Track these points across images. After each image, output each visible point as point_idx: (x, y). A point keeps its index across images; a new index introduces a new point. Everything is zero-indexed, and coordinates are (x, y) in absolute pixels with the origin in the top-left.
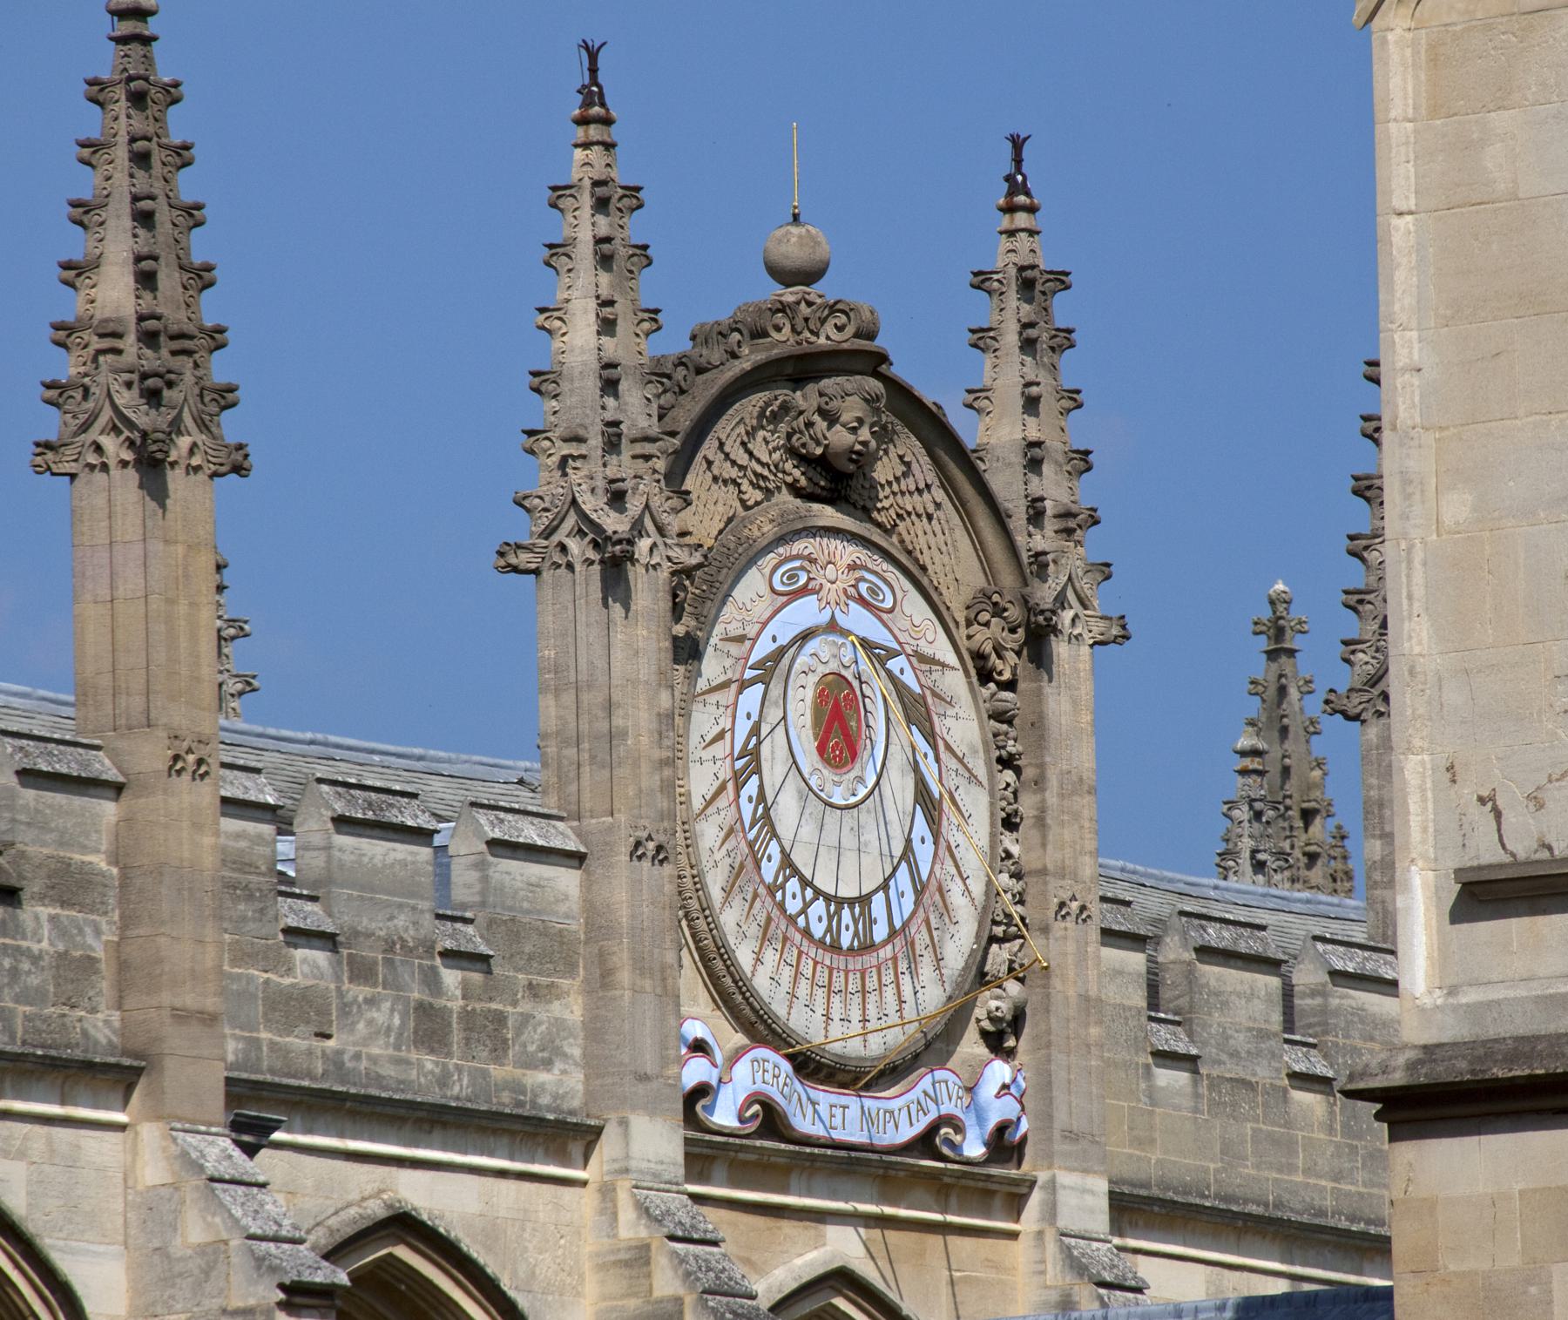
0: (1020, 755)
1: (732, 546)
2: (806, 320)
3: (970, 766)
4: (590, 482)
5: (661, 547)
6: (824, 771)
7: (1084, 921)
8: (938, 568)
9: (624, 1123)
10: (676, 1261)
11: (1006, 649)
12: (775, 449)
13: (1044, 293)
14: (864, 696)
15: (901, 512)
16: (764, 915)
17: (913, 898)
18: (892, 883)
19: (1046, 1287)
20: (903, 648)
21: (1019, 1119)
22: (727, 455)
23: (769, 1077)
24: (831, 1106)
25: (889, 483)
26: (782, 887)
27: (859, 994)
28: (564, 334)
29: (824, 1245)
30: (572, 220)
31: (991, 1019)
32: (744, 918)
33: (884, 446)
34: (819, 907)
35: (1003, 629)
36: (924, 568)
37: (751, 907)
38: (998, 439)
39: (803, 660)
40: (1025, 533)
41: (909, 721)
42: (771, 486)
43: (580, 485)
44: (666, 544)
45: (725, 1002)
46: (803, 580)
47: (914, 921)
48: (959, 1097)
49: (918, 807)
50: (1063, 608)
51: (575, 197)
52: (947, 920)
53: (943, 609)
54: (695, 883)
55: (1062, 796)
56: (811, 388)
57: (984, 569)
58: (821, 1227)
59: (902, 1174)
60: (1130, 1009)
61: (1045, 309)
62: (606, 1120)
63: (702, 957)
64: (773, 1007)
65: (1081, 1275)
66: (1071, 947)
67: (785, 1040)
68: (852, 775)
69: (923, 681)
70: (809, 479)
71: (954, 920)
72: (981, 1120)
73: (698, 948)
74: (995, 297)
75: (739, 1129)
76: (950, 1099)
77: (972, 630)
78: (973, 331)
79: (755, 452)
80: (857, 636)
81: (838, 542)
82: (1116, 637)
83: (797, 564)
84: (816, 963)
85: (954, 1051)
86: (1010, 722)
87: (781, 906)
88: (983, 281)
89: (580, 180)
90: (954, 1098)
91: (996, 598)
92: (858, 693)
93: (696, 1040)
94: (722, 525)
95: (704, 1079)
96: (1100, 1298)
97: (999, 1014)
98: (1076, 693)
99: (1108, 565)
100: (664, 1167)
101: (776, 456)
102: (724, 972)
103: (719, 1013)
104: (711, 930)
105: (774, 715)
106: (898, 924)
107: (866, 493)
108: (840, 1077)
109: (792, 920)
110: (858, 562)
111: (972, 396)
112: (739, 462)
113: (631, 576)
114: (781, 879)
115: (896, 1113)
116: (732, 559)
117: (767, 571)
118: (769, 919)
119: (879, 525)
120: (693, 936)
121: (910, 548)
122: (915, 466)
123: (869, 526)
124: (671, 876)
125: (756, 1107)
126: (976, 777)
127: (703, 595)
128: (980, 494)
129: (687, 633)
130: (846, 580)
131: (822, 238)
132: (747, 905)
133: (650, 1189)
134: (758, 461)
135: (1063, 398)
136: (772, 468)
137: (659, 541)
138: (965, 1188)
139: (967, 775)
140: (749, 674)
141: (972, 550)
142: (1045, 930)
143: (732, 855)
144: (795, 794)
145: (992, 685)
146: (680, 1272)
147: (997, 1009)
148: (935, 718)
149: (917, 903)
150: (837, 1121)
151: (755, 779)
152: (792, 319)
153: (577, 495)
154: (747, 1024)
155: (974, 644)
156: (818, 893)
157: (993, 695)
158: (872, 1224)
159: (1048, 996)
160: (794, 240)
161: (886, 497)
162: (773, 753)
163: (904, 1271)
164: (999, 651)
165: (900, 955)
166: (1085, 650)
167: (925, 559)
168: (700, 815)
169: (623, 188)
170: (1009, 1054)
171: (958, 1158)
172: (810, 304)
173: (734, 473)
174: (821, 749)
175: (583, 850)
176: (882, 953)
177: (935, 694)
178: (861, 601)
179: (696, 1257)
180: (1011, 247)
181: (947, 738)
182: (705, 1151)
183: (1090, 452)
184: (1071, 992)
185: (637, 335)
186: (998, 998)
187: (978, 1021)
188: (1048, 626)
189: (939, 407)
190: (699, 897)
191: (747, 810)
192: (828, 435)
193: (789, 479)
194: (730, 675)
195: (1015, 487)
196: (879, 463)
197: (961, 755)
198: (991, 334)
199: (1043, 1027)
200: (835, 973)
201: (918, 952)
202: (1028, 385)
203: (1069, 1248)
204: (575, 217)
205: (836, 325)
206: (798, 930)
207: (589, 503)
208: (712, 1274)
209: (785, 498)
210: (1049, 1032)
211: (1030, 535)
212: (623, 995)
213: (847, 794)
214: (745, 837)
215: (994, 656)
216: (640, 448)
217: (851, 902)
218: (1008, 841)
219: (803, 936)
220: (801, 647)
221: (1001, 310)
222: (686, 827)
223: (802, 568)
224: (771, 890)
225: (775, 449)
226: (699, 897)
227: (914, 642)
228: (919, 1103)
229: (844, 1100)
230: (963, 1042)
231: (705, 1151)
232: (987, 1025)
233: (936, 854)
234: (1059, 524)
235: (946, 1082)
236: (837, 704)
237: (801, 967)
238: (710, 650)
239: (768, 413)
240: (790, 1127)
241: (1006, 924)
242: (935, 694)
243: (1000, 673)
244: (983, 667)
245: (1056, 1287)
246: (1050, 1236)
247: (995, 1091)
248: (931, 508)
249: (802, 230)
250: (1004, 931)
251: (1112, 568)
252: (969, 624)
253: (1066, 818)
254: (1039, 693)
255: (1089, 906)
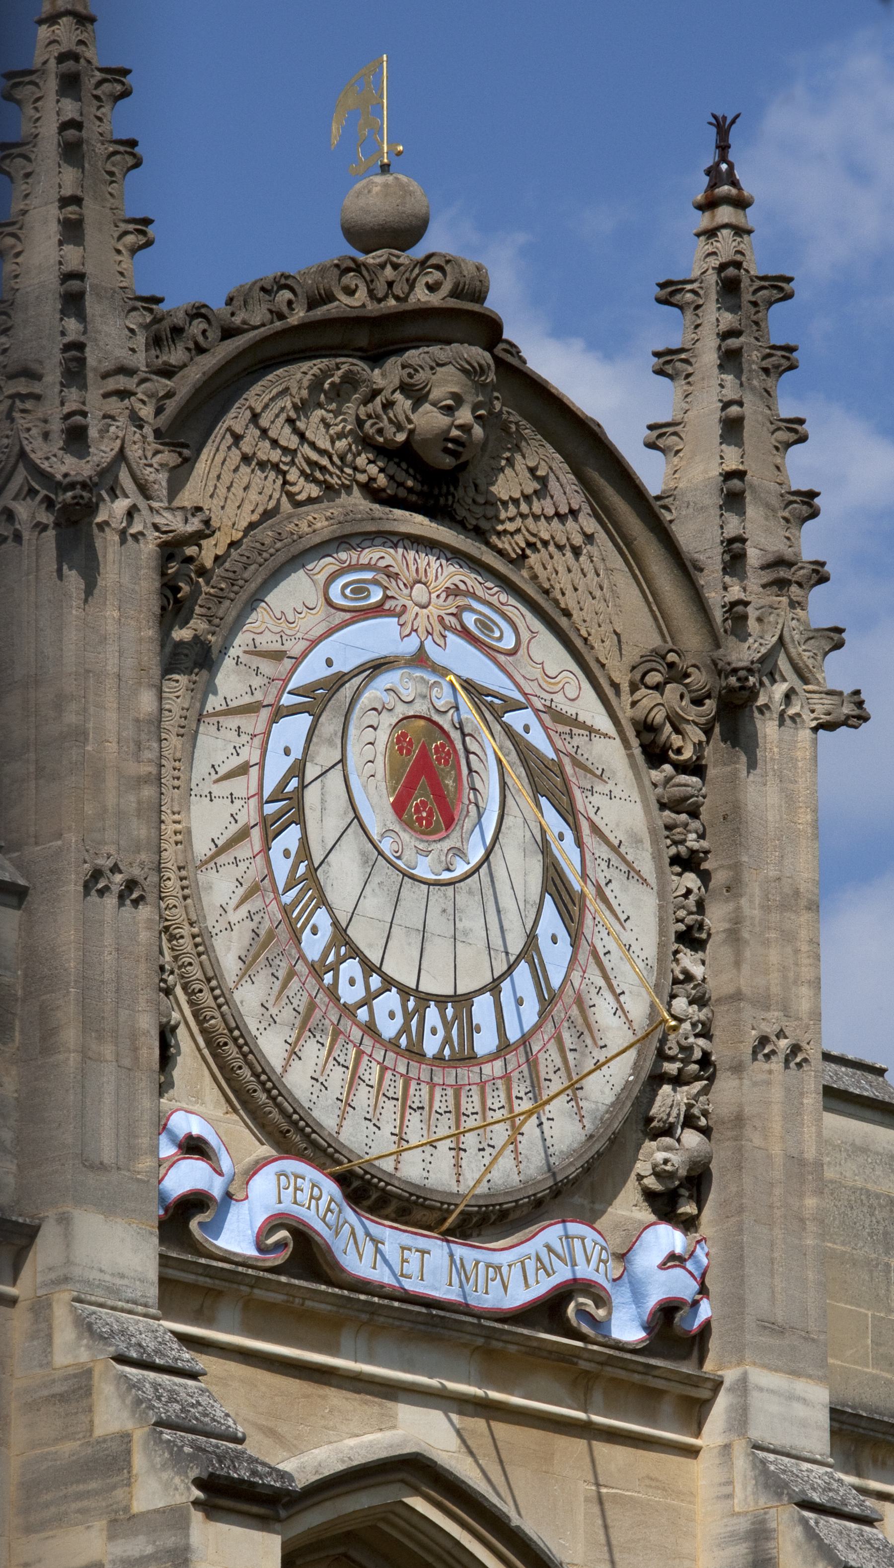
0: (706, 852)
1: (267, 541)
2: (390, 284)
3: (629, 858)
4: (42, 425)
5: (145, 512)
6: (401, 834)
7: (799, 1065)
8: (587, 615)
9: (64, 1220)
10: (124, 1387)
11: (688, 722)
12: (340, 436)
13: (755, 304)
14: (467, 752)
15: (532, 539)
16: (305, 999)
17: (537, 1008)
18: (506, 985)
19: (734, 1514)
20: (528, 700)
21: (695, 1304)
22: (264, 432)
23: (301, 1197)
24: (403, 1248)
25: (516, 502)
26: (334, 968)
27: (452, 1116)
28: (18, 255)
29: (394, 1427)
30: (32, 112)
31: (658, 1174)
32: (272, 999)
33: (507, 454)
34: (391, 999)
35: (682, 697)
36: (567, 613)
37: (284, 986)
38: (689, 481)
39: (375, 693)
40: (721, 586)
41: (537, 791)
42: (334, 481)
43: (29, 430)
44: (151, 509)
45: (244, 1103)
46: (376, 595)
47: (539, 1035)
48: (600, 1260)
49: (547, 897)
50: (773, 681)
51: (36, 85)
52: (589, 1041)
53: (579, 643)
54: (196, 945)
55: (766, 909)
56: (393, 365)
57: (659, 627)
58: (389, 1404)
59: (513, 1348)
60: (878, 1196)
61: (756, 323)
62: (42, 1219)
63: (208, 1043)
64: (315, 1114)
65: (779, 1495)
66: (777, 1094)
67: (331, 1156)
68: (446, 845)
69: (559, 744)
70: (391, 478)
71: (601, 1043)
72: (637, 1296)
73: (203, 1031)
74: (689, 313)
75: (256, 1259)
76: (588, 1261)
77: (638, 695)
78: (657, 354)
79: (308, 434)
80: (458, 677)
81: (432, 559)
82: (848, 717)
83: (368, 575)
84: (384, 1069)
85: (603, 1212)
86: (694, 814)
87: (332, 992)
88: (672, 293)
89: (45, 63)
90: (594, 1259)
91: (671, 657)
92: (459, 746)
93: (190, 1137)
94: (255, 517)
95: (200, 1185)
96: (804, 1522)
97: (668, 1168)
98: (791, 786)
99: (839, 631)
100: (125, 1282)
101: (342, 444)
102: (241, 1062)
103: (235, 1117)
104: (219, 1006)
105: (326, 755)
106: (513, 1035)
107: (479, 510)
108: (418, 1214)
109: (349, 1011)
110: (462, 587)
111: (656, 433)
112: (283, 442)
113: (98, 544)
114: (331, 958)
115: (505, 1270)
116: (265, 555)
117: (321, 578)
118: (312, 1006)
119: (501, 553)
120: (195, 1015)
121: (546, 585)
122: (553, 484)
123: (484, 548)
124: (150, 920)
125: (283, 1234)
126: (638, 873)
127: (220, 594)
128: (652, 530)
129: (196, 637)
130: (440, 607)
131: (415, 186)
132: (278, 984)
133: (101, 1305)
134: (313, 445)
135: (779, 429)
136: (335, 459)
137: (142, 503)
138: (616, 1382)
139: (624, 868)
140: (287, 700)
141: (650, 621)
142: (738, 1069)
143: (257, 918)
144: (358, 857)
145: (667, 767)
146: (129, 1400)
147: (666, 1162)
148: (577, 793)
149: (543, 1014)
150: (413, 1267)
151: (294, 831)
152: (369, 283)
153: (25, 442)
154: (277, 1134)
155: (639, 713)
156: (389, 983)
157: (668, 780)
158: (470, 1408)
159: (740, 1150)
160: (376, 189)
161: (511, 519)
162: (323, 801)
163: (520, 1476)
164: (677, 724)
165: (515, 1075)
166: (805, 734)
167: (569, 601)
168: (206, 862)
169: (101, 70)
170: (688, 1224)
171: (601, 1339)
172: (395, 267)
173: (275, 456)
174: (399, 807)
175: (22, 882)
176: (487, 1069)
177: (576, 763)
178: (465, 633)
179: (156, 1386)
180: (711, 250)
181: (596, 819)
182: (202, 1280)
183: (817, 494)
184: (776, 1150)
185: (119, 252)
186: (668, 1149)
187: (640, 1178)
188: (743, 688)
189: (599, 425)
190: (201, 963)
191: (282, 869)
192: (412, 417)
193: (362, 478)
194: (258, 696)
195: (709, 536)
196: (501, 476)
197: (616, 843)
198: (683, 356)
199: (734, 1189)
200: (413, 1085)
201: (543, 1075)
202: (726, 405)
203: (763, 1462)
204: (36, 109)
205: (427, 284)
206: (358, 1024)
207: (38, 451)
208: (177, 1407)
209: (357, 501)
210: (740, 1194)
211: (725, 588)
212: (68, 1059)
213: (439, 868)
214: (277, 898)
215: (668, 728)
216: (113, 384)
217: (441, 1001)
218: (689, 961)
219: (364, 1032)
220: (370, 679)
221: (697, 326)
222: (183, 873)
223: (375, 582)
224: (317, 970)
225: (340, 436)
226: (201, 963)
227: (548, 697)
228: (539, 1259)
229: (422, 1243)
230: (618, 1201)
231: (202, 1280)
232: (651, 1182)
233: (574, 959)
234: (768, 576)
235: (583, 1239)
236: (424, 753)
237: (361, 1071)
238: (228, 663)
239: (326, 386)
240: (336, 1265)
241: (682, 1060)
242: (576, 763)
243: (679, 751)
244: (654, 742)
245: (745, 1513)
246: (740, 1449)
247: (659, 1260)
248: (578, 540)
249: (389, 178)
250: (680, 1070)
251: (844, 635)
252: (634, 688)
253: (773, 935)
254: (733, 780)
255: (804, 1045)
